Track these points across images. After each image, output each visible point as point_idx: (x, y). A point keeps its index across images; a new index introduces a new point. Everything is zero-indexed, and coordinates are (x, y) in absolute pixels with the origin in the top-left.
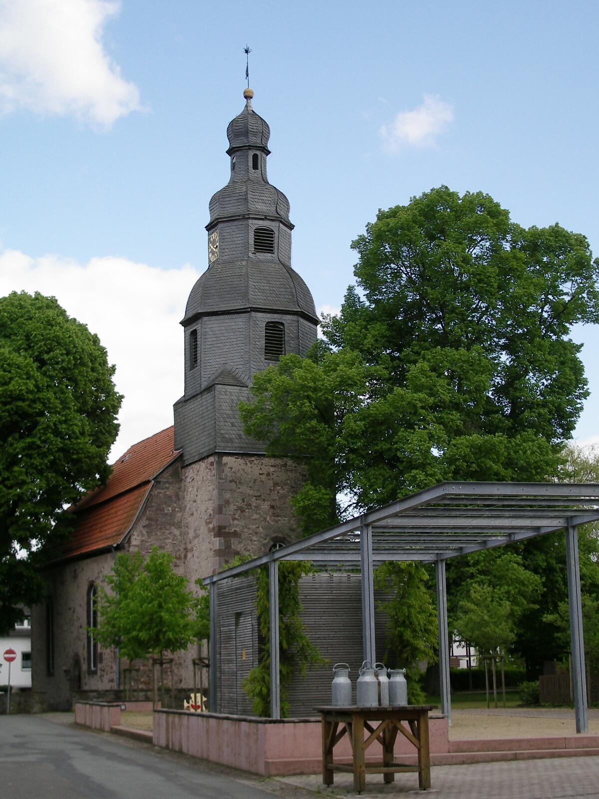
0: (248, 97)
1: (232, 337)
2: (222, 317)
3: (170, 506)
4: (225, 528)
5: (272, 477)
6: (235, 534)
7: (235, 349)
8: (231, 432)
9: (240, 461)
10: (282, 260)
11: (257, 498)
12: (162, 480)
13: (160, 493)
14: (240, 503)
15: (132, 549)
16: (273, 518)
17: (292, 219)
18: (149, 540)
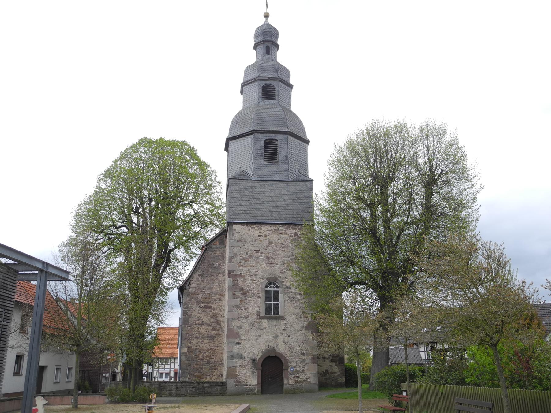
0: (267, 16)
1: (244, 151)
2: (239, 139)
3: (217, 263)
4: (233, 271)
5: (268, 237)
6: (241, 276)
7: (246, 157)
8: (239, 209)
9: (245, 227)
10: (281, 104)
11: (257, 252)
12: (212, 246)
13: (211, 254)
14: (244, 255)
15: (191, 289)
16: (268, 265)
17: (292, 81)
18: (203, 284)
